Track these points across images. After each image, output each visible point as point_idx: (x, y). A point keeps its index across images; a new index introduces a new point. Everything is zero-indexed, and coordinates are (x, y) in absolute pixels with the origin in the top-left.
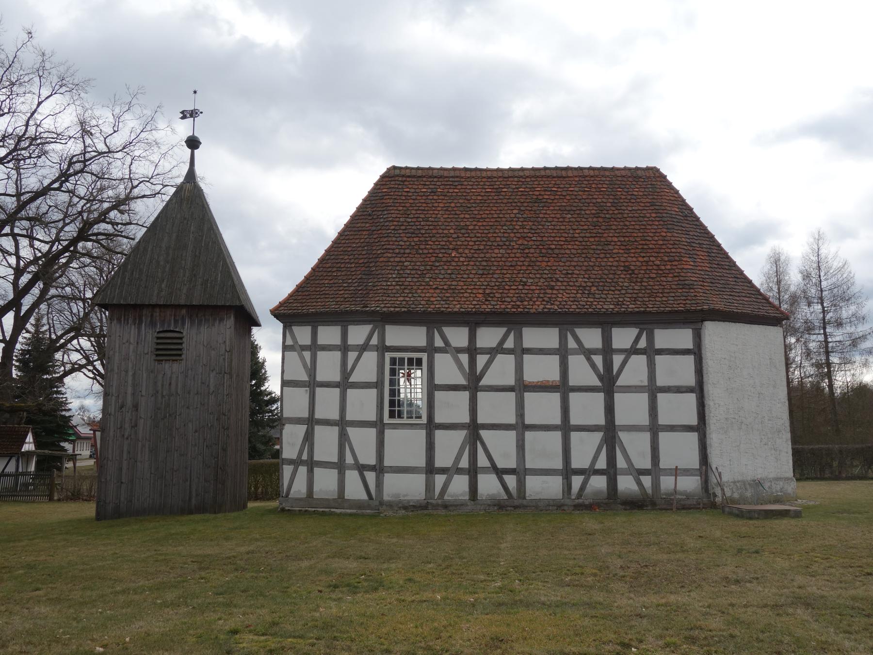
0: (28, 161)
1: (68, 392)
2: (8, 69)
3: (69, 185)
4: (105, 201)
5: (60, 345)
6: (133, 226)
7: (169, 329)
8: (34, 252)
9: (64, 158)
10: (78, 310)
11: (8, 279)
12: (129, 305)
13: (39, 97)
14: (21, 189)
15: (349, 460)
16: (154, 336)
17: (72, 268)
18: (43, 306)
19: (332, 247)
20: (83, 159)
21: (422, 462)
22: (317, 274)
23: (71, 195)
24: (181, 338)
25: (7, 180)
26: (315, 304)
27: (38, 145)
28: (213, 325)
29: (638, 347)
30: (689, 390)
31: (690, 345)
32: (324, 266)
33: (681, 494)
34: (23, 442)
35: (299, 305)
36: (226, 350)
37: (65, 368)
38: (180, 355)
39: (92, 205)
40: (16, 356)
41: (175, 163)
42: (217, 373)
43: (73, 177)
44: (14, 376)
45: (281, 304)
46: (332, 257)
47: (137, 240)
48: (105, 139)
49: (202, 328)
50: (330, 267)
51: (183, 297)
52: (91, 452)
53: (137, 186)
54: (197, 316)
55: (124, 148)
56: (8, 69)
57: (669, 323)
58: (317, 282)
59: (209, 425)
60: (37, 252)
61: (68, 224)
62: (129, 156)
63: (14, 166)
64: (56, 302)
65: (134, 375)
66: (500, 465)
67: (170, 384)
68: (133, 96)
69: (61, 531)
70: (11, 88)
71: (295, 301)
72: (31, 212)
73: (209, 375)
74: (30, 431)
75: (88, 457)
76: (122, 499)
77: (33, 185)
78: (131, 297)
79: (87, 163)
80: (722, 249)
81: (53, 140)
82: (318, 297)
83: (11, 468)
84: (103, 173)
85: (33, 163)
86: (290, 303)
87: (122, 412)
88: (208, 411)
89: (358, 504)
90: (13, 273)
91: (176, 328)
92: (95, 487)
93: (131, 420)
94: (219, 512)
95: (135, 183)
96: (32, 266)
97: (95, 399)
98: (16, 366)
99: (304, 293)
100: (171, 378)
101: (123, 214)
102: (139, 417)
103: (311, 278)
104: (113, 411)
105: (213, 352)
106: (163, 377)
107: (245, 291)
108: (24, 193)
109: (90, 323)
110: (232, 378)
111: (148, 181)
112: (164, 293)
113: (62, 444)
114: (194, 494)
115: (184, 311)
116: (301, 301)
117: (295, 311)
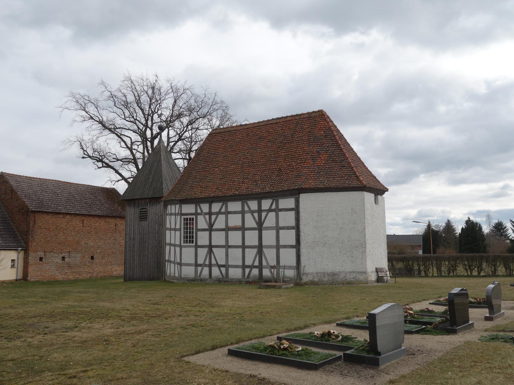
21: (193, 262)
29: (272, 208)
30: (292, 228)
31: (293, 206)
33: (288, 278)
38: (147, 218)
57: (284, 196)
66: (219, 263)
80: (354, 151)
115: (148, 200)
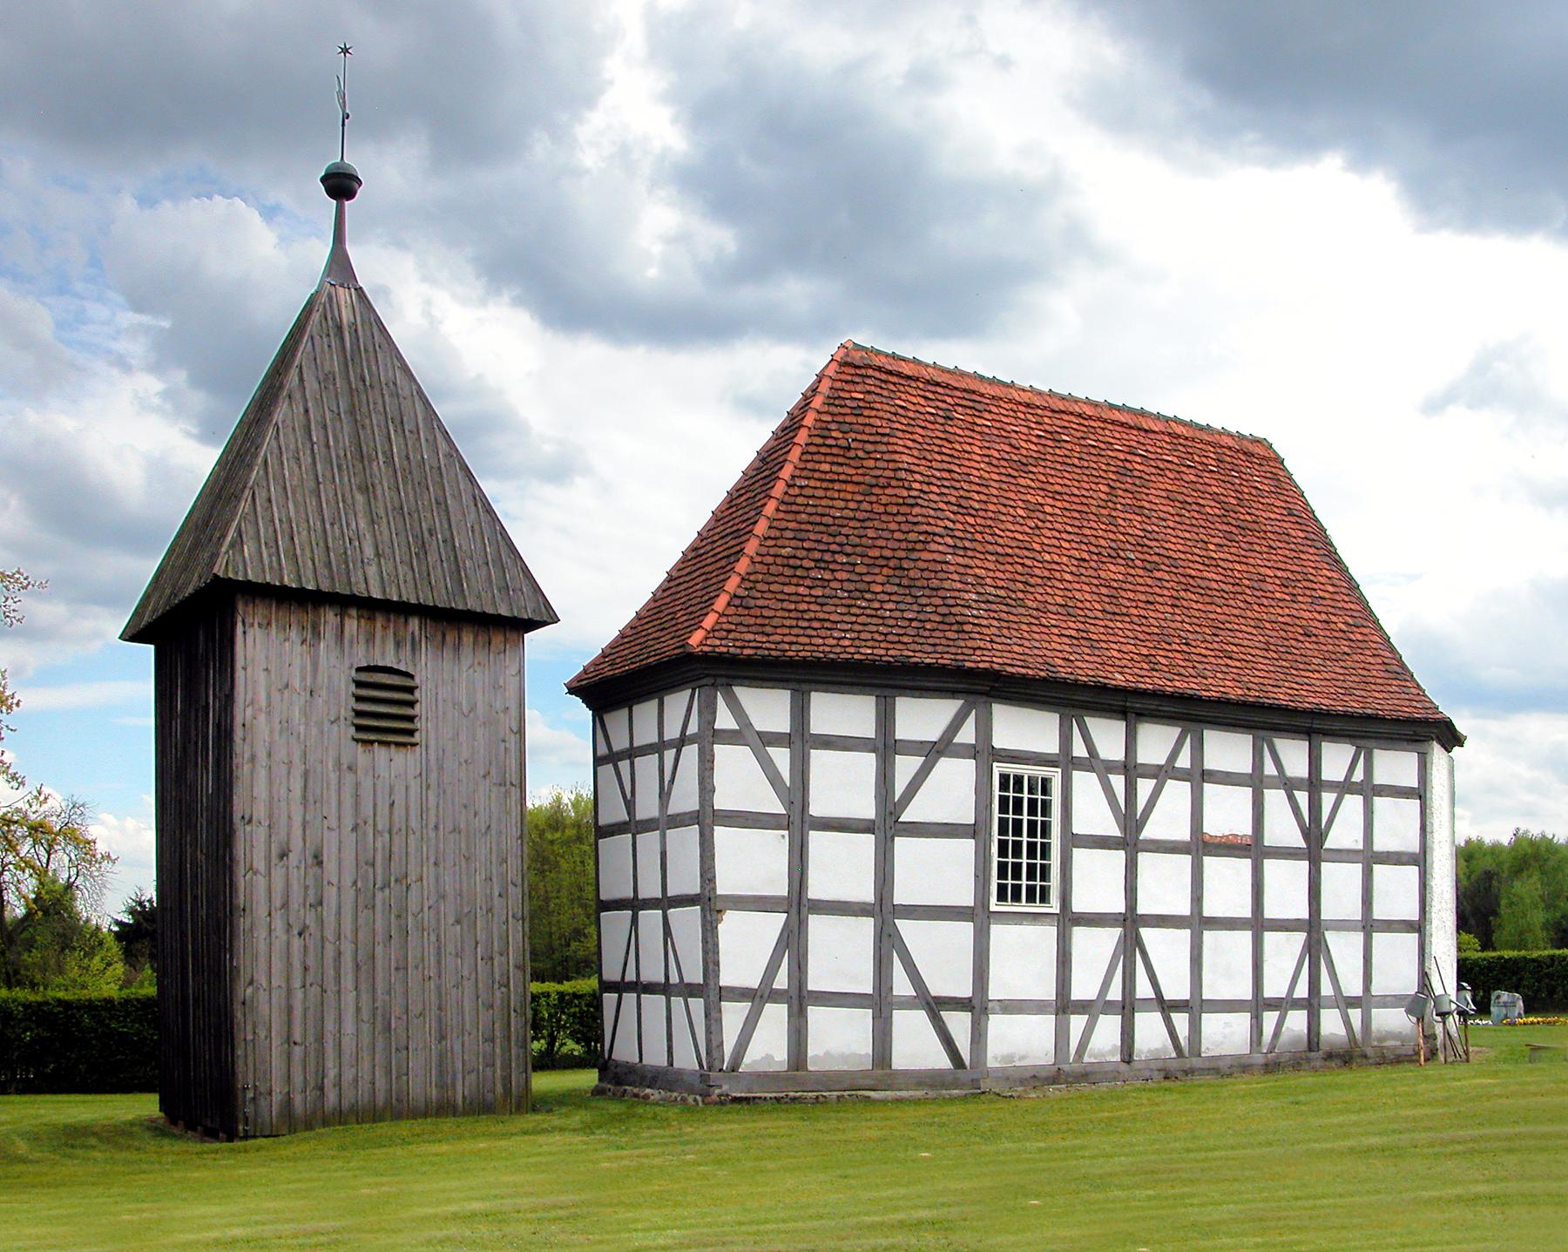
15: (902, 986)
21: (1048, 992)
24: (411, 690)
38: (411, 733)
57: (1392, 739)
89: (928, 1080)
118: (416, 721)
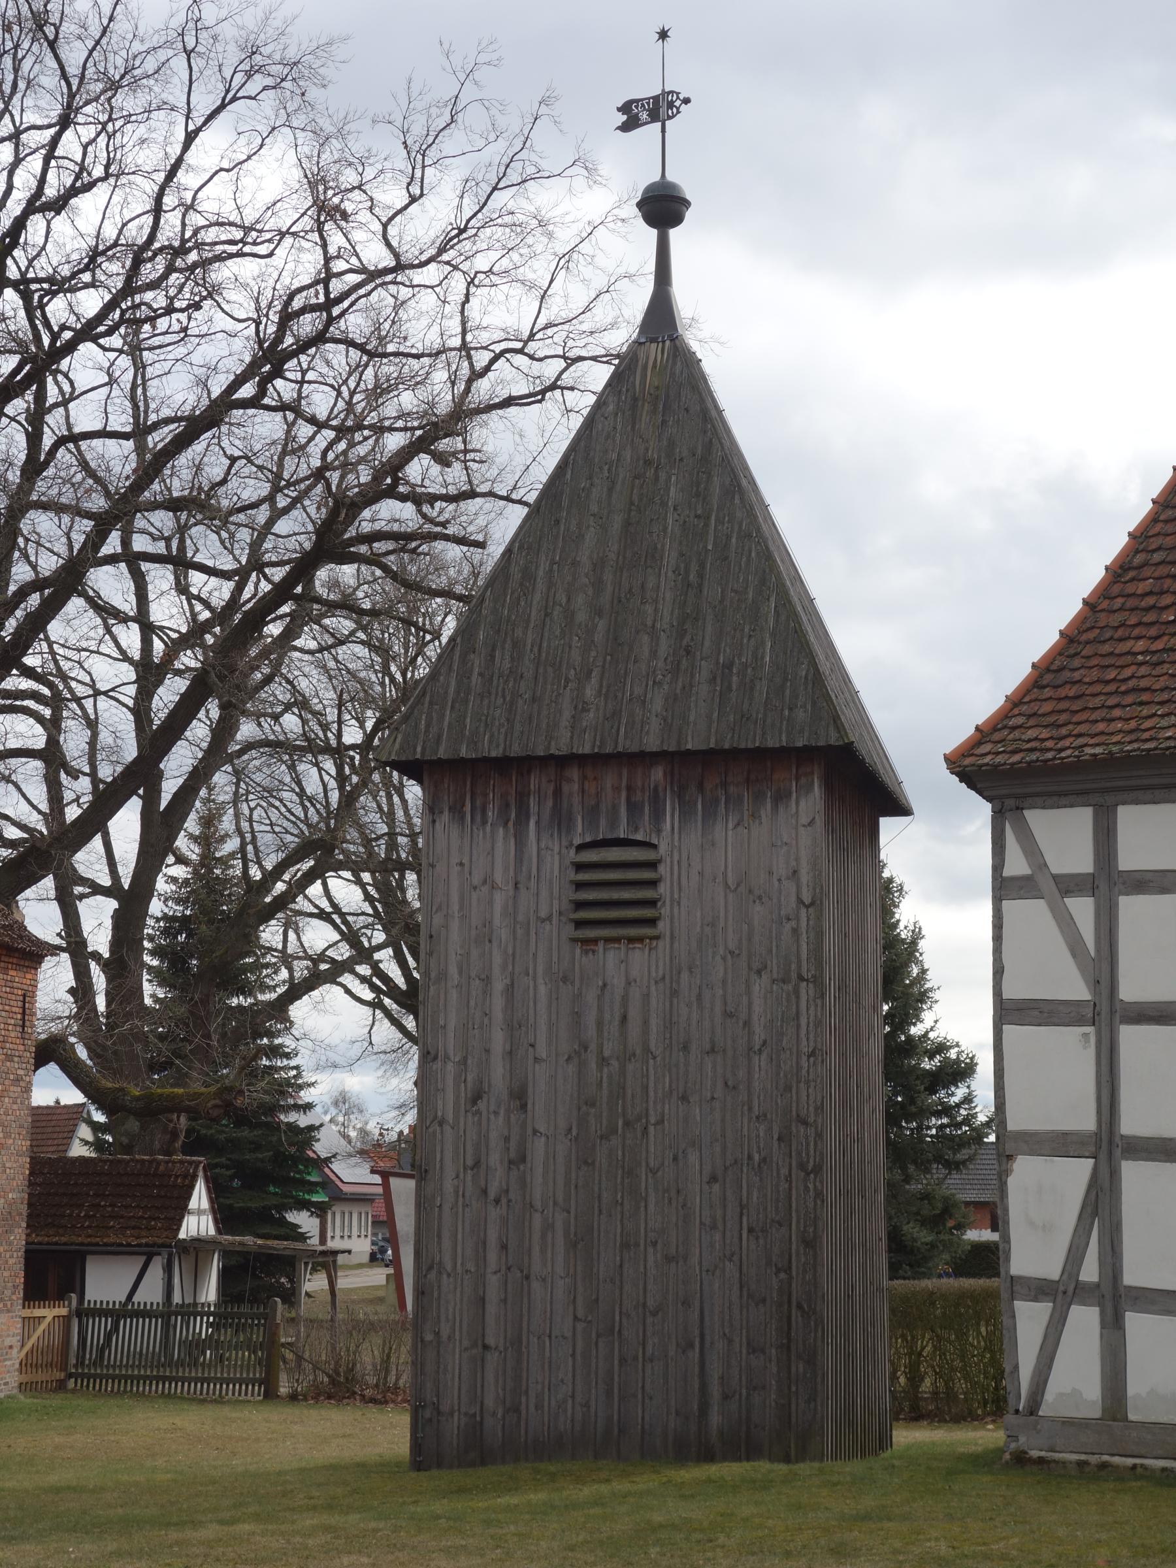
0: (162, 323)
1: (302, 1051)
2: (98, 43)
3: (283, 388)
4: (391, 429)
5: (275, 898)
6: (479, 501)
7: (614, 836)
8: (191, 606)
9: (264, 304)
10: (325, 786)
11: (122, 698)
12: (486, 760)
13: (188, 117)
14: (146, 412)
16: (567, 862)
17: (301, 650)
18: (221, 778)
19: (1153, 519)
20: (322, 299)
22: (1103, 619)
23: (290, 416)
24: (652, 865)
25: (106, 389)
26: (1101, 726)
27: (192, 268)
28: (754, 816)
32: (1130, 588)
34: (181, 1209)
35: (1045, 734)
36: (800, 901)
37: (291, 970)
38: (652, 922)
39: (352, 445)
40: (151, 939)
41: (600, 282)
42: (774, 981)
43: (295, 361)
44: (148, 1001)
45: (983, 734)
46: (1157, 557)
47: (496, 550)
48: (385, 226)
49: (718, 831)
50: (1150, 593)
51: (655, 725)
52: (373, 1243)
53: (487, 369)
54: (701, 787)
55: (442, 250)
56: (98, 43)
58: (1106, 648)
59: (756, 1157)
60: (198, 607)
61: (286, 511)
62: (458, 275)
63: (125, 343)
64: (257, 763)
65: (510, 990)
67: (624, 1019)
68: (462, 77)
69: (311, 1498)
70: (109, 100)
71: (1031, 722)
72: (176, 483)
73: (748, 986)
74: (201, 1174)
75: (366, 1258)
76: (489, 1402)
77: (179, 398)
78: (492, 736)
79: (336, 311)
81: (233, 249)
82: (1112, 701)
83: (150, 1293)
84: (381, 339)
85: (176, 327)
86: (1014, 728)
87: (478, 1112)
88: (750, 1109)
90: (133, 677)
91: (636, 829)
92: (403, 1355)
93: (507, 1139)
94: (802, 1456)
95: (481, 359)
96: (189, 652)
97: (380, 1073)
98: (150, 969)
99: (1062, 692)
100: (625, 999)
101: (448, 465)
102: (529, 1131)
103: (1084, 637)
104: (450, 1106)
105: (758, 907)
106: (600, 997)
107: (854, 695)
108: (156, 426)
109: (361, 827)
110: (822, 996)
111: (520, 351)
112: (591, 715)
113: (293, 1217)
114: (715, 1392)
115: (658, 774)
116: (1051, 719)
117: (1034, 757)
118: (659, 904)
